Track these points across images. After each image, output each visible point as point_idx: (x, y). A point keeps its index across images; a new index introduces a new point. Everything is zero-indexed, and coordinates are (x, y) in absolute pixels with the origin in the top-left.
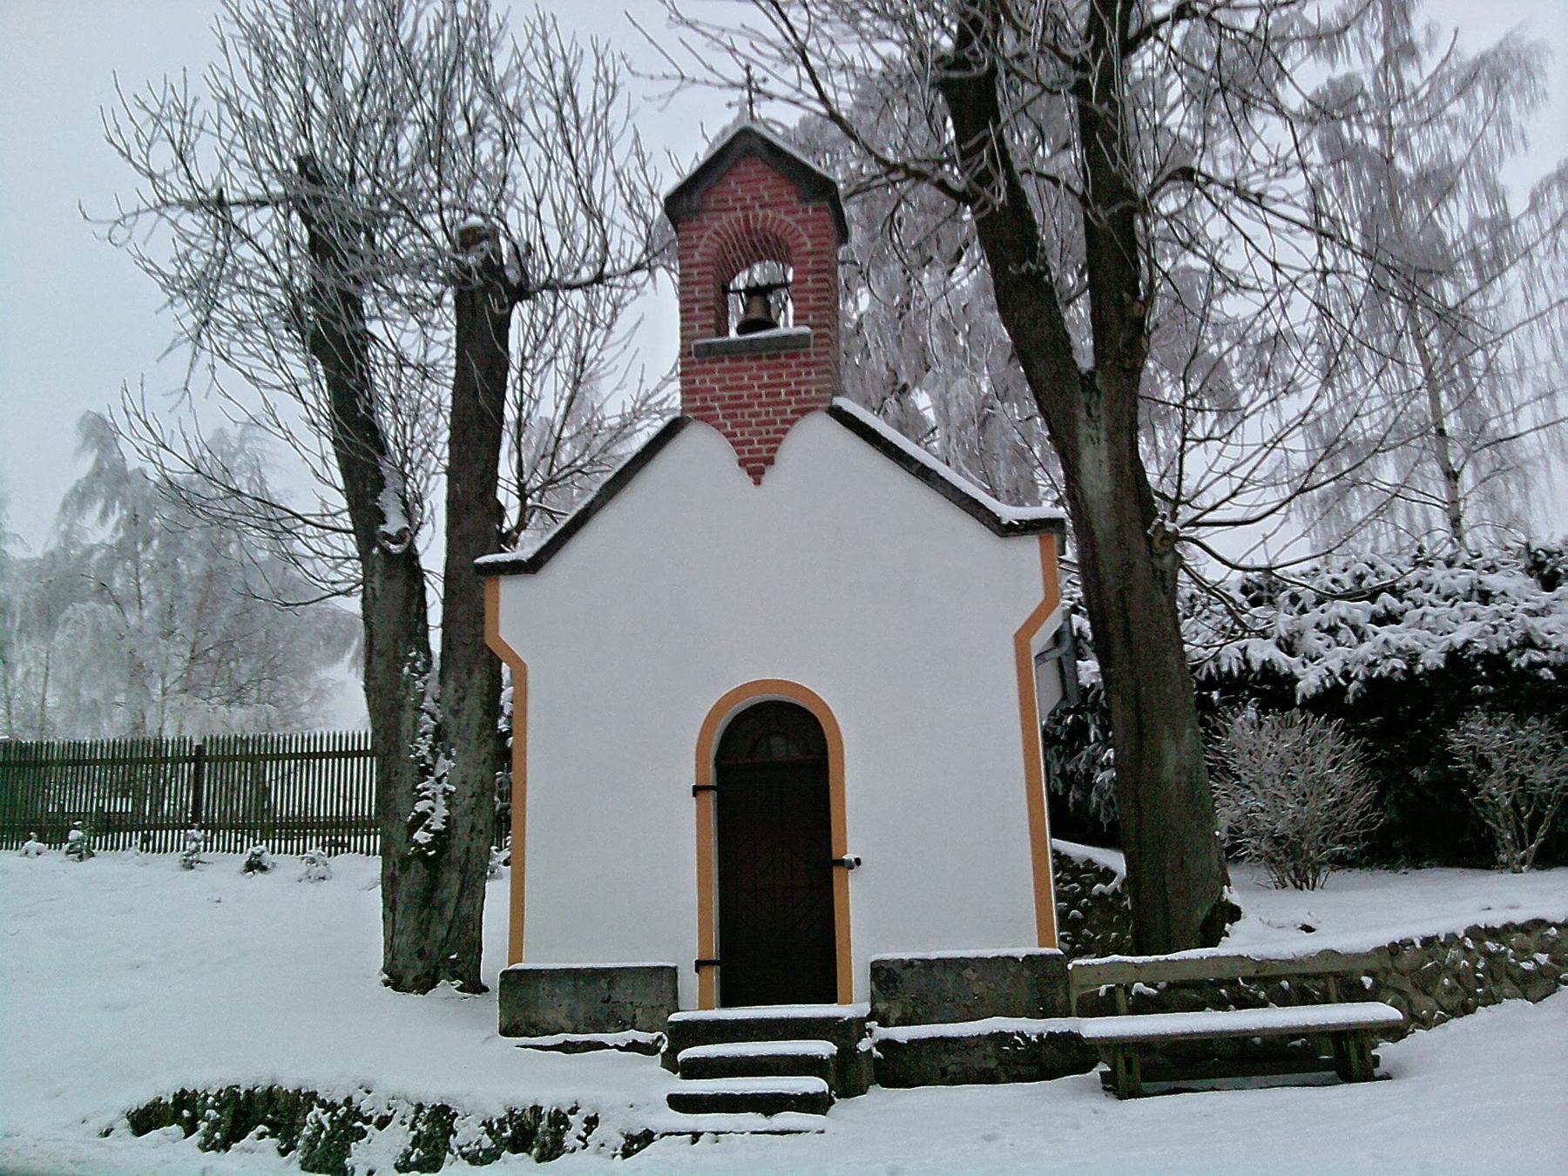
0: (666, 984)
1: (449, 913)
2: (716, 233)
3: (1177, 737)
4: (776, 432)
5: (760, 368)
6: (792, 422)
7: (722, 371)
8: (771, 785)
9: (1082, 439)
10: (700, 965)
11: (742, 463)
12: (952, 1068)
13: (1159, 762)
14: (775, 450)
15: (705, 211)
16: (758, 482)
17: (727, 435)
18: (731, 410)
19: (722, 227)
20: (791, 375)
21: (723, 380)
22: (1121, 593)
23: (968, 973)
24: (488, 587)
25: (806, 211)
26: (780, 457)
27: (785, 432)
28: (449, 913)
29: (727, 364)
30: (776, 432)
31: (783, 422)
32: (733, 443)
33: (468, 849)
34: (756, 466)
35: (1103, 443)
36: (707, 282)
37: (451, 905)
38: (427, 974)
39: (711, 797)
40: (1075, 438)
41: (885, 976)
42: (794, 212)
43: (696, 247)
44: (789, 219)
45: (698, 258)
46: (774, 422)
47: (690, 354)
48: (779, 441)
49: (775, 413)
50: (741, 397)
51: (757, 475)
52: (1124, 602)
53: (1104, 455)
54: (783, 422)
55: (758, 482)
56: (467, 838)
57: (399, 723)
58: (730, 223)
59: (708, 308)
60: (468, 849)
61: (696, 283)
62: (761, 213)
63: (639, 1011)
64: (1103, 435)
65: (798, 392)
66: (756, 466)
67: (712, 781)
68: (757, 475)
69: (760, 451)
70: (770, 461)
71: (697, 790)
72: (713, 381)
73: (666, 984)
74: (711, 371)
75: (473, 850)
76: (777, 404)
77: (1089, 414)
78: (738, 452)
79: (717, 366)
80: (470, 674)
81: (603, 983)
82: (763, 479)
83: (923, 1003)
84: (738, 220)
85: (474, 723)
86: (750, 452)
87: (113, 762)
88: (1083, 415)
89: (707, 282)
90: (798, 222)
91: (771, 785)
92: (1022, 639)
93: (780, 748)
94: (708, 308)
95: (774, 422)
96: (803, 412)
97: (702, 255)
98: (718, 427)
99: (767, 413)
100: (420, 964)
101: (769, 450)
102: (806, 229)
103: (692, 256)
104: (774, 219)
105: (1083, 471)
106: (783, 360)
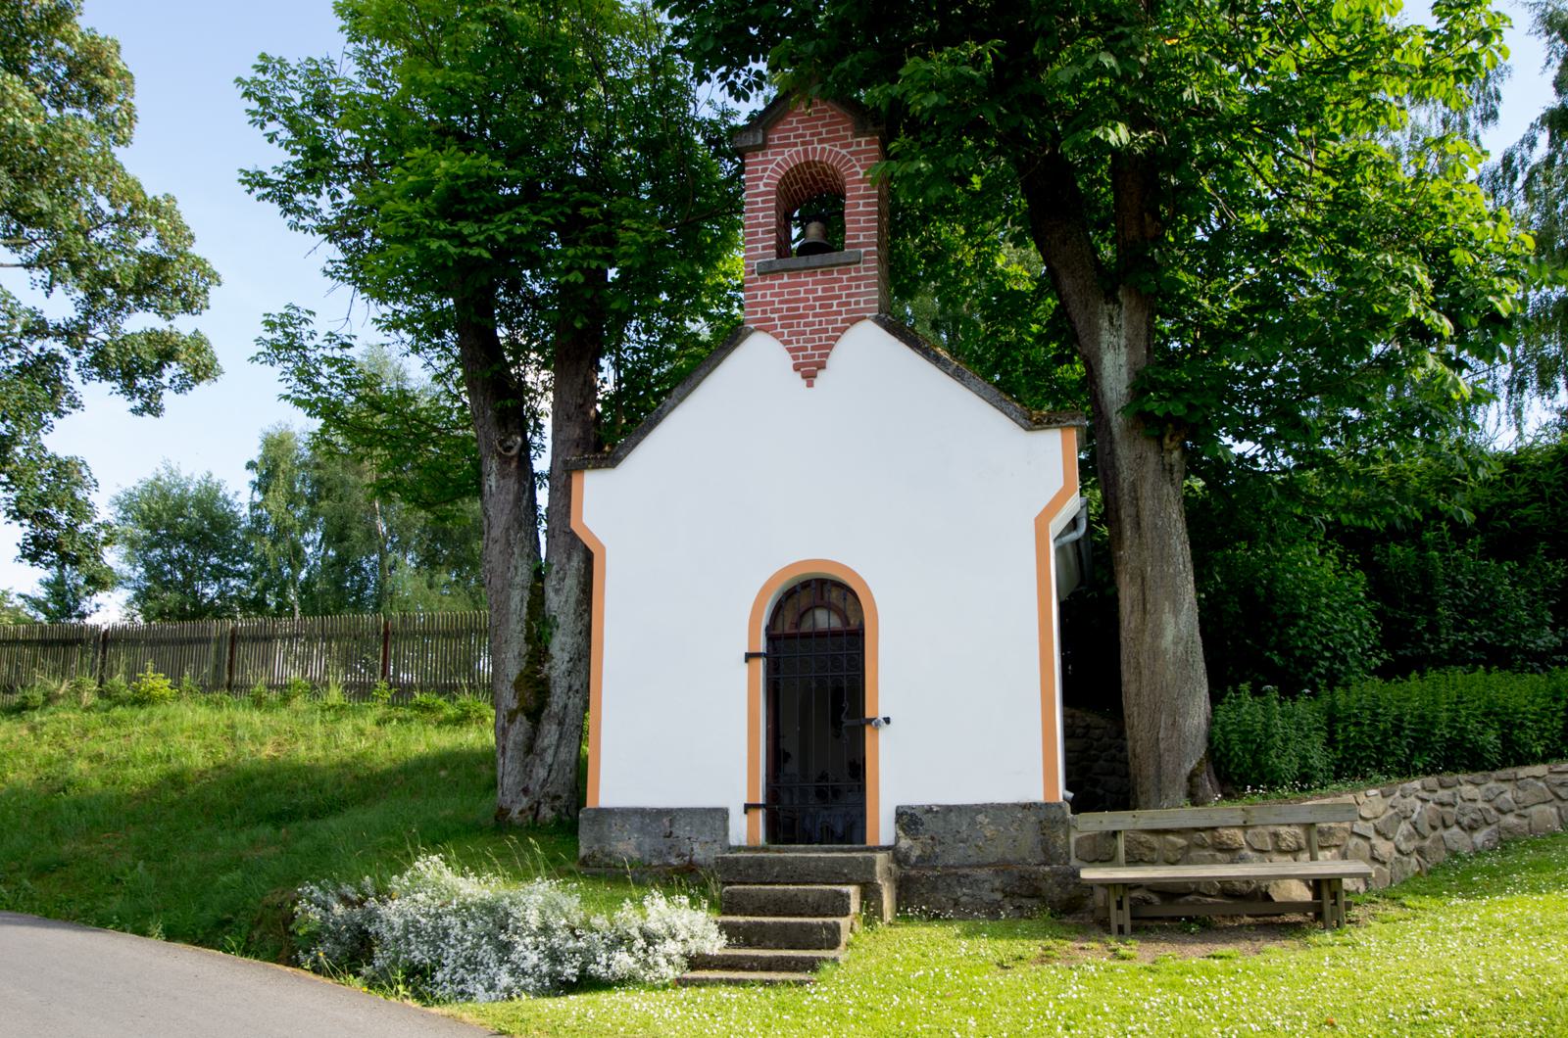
0: (718, 823)
1: (549, 759)
2: (778, 165)
3: (1176, 612)
4: (827, 339)
5: (815, 283)
6: (843, 330)
7: (781, 286)
8: (815, 659)
9: (1104, 346)
10: (748, 808)
11: (797, 368)
12: (963, 899)
13: (1157, 634)
14: (827, 355)
15: (770, 147)
16: (810, 385)
17: (785, 343)
18: (788, 320)
19: (784, 160)
20: (841, 288)
21: (782, 294)
22: (1133, 484)
23: (980, 818)
24: (575, 478)
25: (859, 144)
26: (831, 362)
27: (836, 339)
28: (549, 759)
29: (786, 280)
30: (827, 339)
31: (834, 330)
32: (790, 350)
33: (566, 706)
34: (809, 369)
35: (1123, 349)
36: (769, 209)
37: (551, 752)
38: (531, 808)
39: (761, 663)
40: (1098, 344)
41: (908, 819)
42: (850, 145)
43: (761, 178)
44: (844, 152)
45: (762, 188)
46: (826, 331)
47: (753, 272)
48: (831, 347)
49: (827, 322)
50: (798, 309)
51: (809, 377)
52: (1136, 491)
53: (1123, 359)
54: (834, 330)
55: (810, 385)
56: (564, 697)
57: (508, 598)
58: (791, 156)
59: (769, 232)
60: (566, 706)
61: (760, 225)
62: (819, 147)
63: (696, 846)
64: (1123, 342)
65: (849, 304)
66: (809, 369)
67: (761, 801)
68: (809, 377)
69: (813, 356)
70: (822, 366)
71: (749, 657)
72: (772, 295)
73: (718, 823)
74: (772, 287)
75: (570, 706)
76: (828, 314)
77: (1111, 323)
78: (795, 358)
79: (777, 282)
80: (569, 559)
81: (666, 821)
82: (816, 382)
83: (941, 843)
84: (798, 153)
85: (572, 600)
86: (804, 357)
87: (447, 635)
88: (1106, 324)
89: (769, 209)
90: (852, 154)
91: (815, 659)
92: (1041, 522)
93: (824, 620)
94: (769, 232)
95: (826, 331)
96: (854, 321)
97: (766, 185)
98: (776, 336)
99: (820, 339)
100: (525, 800)
101: (821, 356)
102: (858, 160)
103: (757, 186)
104: (831, 151)
105: (1105, 374)
106: (835, 275)
